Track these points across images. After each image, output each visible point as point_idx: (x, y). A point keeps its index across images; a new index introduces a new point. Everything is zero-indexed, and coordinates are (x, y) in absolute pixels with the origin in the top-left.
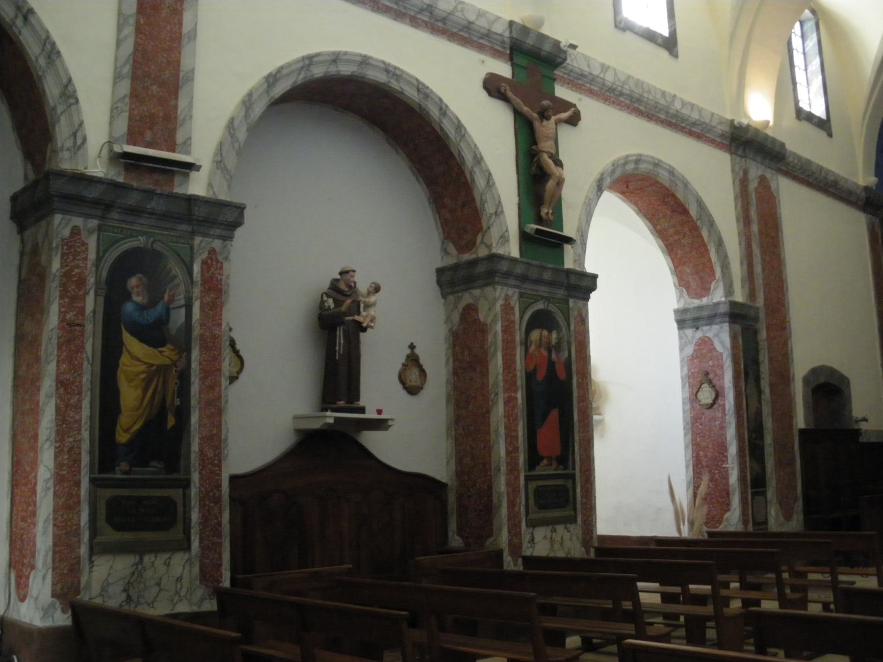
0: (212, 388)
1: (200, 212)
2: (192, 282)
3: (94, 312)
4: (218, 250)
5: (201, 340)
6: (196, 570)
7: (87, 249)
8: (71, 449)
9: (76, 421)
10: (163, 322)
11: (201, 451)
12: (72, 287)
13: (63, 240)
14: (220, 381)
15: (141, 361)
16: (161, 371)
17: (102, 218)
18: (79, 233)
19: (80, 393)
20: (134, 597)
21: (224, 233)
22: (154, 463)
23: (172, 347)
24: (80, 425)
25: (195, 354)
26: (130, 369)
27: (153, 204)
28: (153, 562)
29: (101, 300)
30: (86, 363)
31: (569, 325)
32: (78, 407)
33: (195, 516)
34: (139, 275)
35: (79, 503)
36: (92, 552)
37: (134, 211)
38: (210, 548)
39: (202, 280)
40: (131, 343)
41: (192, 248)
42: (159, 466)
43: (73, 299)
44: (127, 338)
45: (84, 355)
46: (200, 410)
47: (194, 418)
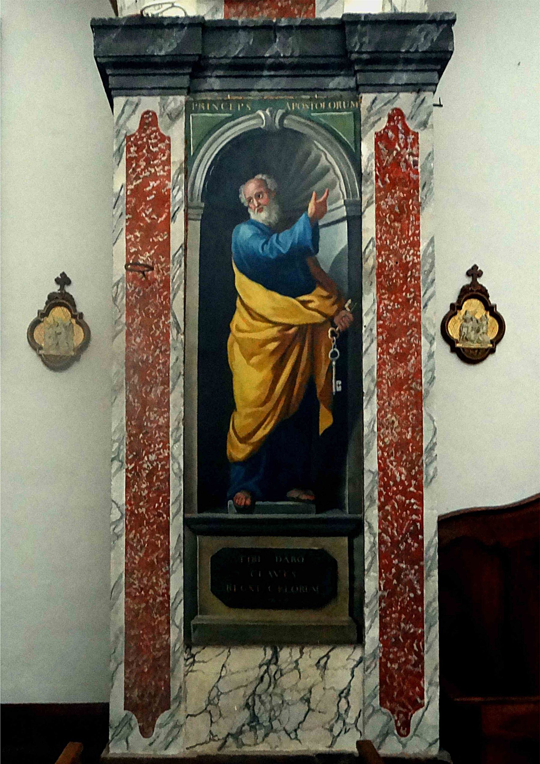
0: (402, 357)
1: (361, 44)
2: (360, 175)
3: (185, 247)
4: (406, 112)
5: (378, 276)
6: (374, 680)
7: (169, 146)
8: (152, 472)
9: (159, 427)
10: (309, 248)
11: (383, 468)
12: (147, 213)
13: (128, 138)
14: (419, 346)
15: (269, 322)
16: (308, 333)
17: (191, 91)
18: (154, 122)
19: (166, 382)
20: (264, 718)
21: (419, 77)
22: (294, 493)
23: (325, 293)
24: (167, 433)
25: (369, 301)
26: (246, 335)
27: (277, 49)
28: (296, 662)
29: (196, 226)
30: (173, 332)
31: (355, 158)
32: (163, 405)
33: (371, 584)
34: (260, 176)
35: (167, 559)
36: (188, 644)
37: (246, 68)
38: (401, 643)
39: (378, 169)
40: (252, 293)
41: (357, 115)
42: (304, 497)
43: (149, 230)
44: (243, 283)
45: (171, 320)
46: (379, 398)
47: (370, 413)
